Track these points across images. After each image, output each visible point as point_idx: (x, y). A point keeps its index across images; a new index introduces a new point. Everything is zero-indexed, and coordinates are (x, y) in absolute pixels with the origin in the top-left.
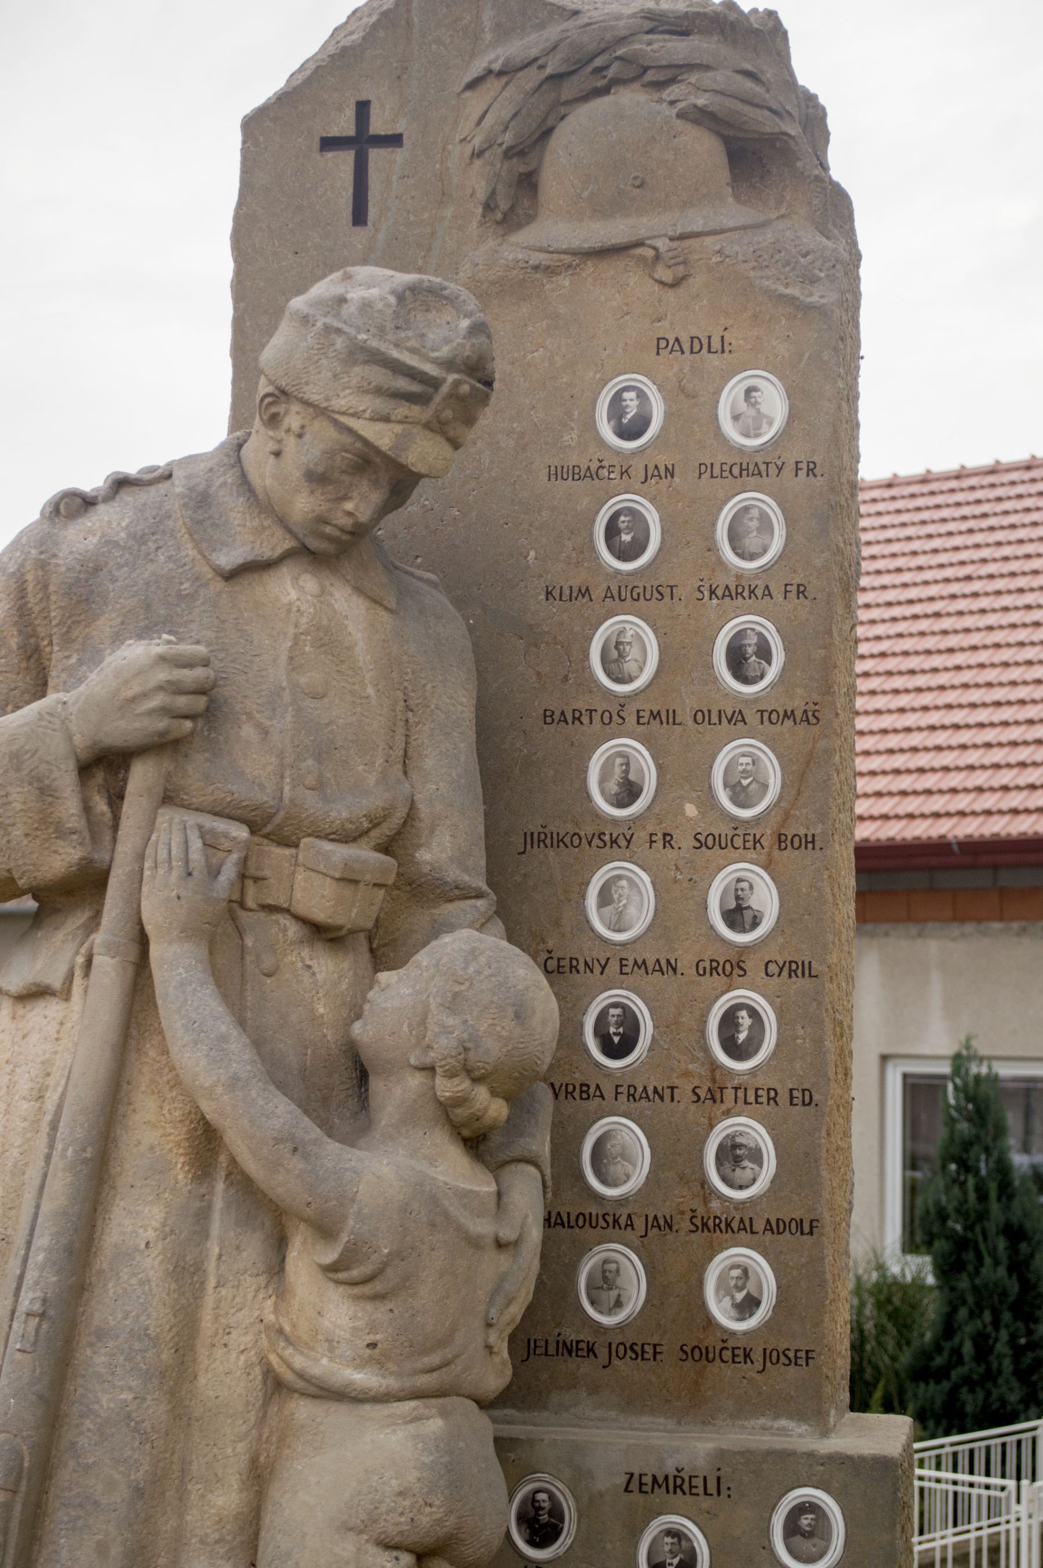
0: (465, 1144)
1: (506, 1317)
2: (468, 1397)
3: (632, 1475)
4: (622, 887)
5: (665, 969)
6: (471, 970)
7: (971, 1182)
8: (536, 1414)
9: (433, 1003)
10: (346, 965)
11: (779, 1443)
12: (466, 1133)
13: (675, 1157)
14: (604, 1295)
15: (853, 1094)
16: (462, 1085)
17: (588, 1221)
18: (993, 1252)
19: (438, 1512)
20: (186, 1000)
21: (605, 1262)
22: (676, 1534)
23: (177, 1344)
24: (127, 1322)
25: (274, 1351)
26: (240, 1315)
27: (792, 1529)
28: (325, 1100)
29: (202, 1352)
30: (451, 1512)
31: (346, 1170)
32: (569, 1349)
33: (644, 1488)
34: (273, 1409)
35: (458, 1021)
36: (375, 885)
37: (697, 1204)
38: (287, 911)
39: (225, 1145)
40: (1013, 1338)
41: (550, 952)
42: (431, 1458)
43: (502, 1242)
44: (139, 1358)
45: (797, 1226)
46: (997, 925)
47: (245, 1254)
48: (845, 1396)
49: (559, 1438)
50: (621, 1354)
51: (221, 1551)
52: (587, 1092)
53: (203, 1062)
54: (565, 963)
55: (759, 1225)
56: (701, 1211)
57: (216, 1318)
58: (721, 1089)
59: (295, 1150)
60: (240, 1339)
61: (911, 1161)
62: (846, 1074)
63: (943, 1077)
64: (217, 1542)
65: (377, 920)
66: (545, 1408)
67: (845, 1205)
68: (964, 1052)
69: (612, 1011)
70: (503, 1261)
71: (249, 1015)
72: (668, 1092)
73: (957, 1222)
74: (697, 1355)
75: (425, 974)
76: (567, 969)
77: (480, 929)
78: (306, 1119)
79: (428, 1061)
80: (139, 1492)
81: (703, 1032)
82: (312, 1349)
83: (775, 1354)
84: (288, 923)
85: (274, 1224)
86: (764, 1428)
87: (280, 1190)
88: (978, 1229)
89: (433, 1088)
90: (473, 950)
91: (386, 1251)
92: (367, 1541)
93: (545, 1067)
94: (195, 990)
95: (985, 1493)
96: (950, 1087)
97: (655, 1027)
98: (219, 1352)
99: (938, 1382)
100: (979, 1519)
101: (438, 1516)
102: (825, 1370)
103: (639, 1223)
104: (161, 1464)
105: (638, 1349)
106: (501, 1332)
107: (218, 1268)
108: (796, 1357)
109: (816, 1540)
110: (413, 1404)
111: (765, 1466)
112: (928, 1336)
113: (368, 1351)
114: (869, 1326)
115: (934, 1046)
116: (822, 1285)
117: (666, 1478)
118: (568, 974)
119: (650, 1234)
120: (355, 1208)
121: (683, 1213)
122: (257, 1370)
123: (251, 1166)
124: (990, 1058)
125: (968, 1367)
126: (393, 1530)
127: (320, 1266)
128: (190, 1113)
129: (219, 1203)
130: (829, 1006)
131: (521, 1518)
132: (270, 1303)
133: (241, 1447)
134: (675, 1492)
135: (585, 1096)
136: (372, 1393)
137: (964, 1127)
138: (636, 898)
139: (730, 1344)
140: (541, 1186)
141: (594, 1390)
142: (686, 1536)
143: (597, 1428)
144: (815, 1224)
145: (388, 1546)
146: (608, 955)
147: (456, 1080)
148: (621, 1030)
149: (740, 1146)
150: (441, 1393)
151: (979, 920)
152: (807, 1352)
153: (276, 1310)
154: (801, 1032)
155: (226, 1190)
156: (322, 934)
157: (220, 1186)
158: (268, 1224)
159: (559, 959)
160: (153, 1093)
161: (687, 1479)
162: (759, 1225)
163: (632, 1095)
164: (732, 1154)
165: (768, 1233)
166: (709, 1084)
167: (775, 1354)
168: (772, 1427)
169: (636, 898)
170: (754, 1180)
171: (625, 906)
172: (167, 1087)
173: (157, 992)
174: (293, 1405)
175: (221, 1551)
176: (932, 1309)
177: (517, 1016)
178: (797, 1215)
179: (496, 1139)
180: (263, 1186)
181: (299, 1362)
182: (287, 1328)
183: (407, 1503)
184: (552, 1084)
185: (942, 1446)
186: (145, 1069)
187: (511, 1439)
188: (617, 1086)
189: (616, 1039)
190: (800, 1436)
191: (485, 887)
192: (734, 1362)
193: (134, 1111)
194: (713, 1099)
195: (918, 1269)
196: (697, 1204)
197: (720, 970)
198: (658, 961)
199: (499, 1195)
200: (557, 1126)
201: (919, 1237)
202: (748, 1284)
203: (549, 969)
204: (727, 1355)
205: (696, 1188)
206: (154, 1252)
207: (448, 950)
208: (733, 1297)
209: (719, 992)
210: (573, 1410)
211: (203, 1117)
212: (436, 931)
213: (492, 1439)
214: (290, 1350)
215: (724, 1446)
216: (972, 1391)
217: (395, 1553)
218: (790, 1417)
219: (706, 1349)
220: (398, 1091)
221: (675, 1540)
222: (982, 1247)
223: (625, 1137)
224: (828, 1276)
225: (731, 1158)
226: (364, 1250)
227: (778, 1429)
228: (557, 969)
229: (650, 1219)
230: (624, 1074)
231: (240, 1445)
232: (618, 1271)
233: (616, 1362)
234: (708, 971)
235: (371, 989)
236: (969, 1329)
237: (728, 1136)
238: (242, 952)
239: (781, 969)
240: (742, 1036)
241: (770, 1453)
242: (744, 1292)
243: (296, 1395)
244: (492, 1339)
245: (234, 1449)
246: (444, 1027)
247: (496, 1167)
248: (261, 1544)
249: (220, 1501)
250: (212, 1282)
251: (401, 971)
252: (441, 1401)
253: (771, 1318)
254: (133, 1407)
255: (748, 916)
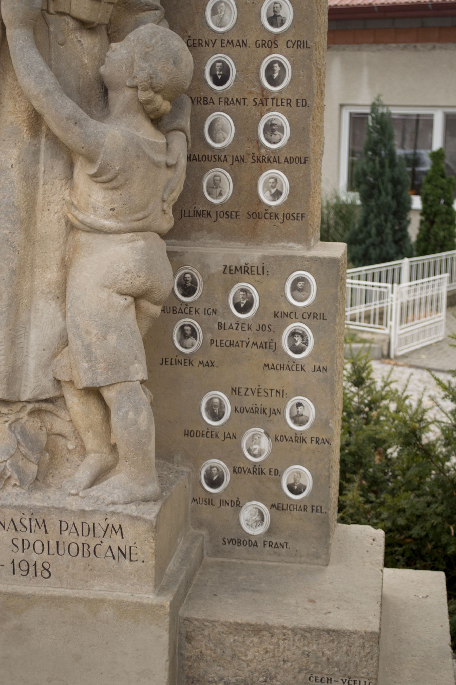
0: (152, 122)
1: (171, 198)
2: (155, 232)
3: (226, 266)
4: (222, 6)
5: (241, 44)
6: (153, 41)
7: (377, 159)
8: (185, 242)
9: (136, 57)
10: (97, 41)
11: (289, 253)
12: (152, 116)
13: (246, 130)
14: (214, 191)
15: (325, 103)
16: (150, 94)
17: (207, 158)
18: (386, 190)
19: (143, 280)
20: (24, 55)
21: (215, 176)
22: (245, 291)
23: (27, 209)
24: (5, 200)
25: (70, 212)
26: (54, 197)
27: (294, 288)
28: (89, 102)
29: (38, 213)
30: (148, 279)
31: (99, 132)
32: (199, 214)
33: (231, 272)
34: (70, 238)
35: (147, 65)
36: (109, 3)
37: (255, 150)
38: (69, 15)
39: (45, 122)
40: (393, 226)
41: (189, 37)
42: (139, 257)
43: (169, 165)
44: (11, 215)
45: (299, 161)
46: (393, 45)
47: (56, 170)
48: (318, 235)
49: (195, 251)
50: (222, 216)
51: (50, 296)
52: (206, 101)
53: (33, 84)
54: (196, 42)
55: (282, 160)
56: (257, 154)
57: (44, 198)
58: (266, 99)
59: (76, 123)
60: (55, 207)
61: (352, 153)
62: (322, 93)
63: (366, 114)
64: (48, 293)
65: (110, 20)
66: (189, 239)
67: (320, 152)
68: (377, 103)
69: (218, 64)
70: (170, 173)
71: (53, 63)
72: (242, 101)
73: (371, 177)
74: (254, 216)
75: (132, 44)
76: (197, 45)
77: (158, 23)
78: (80, 109)
79: (134, 83)
80: (14, 272)
81: (258, 74)
82: (87, 211)
83: (288, 215)
84: (69, 21)
85: (68, 156)
86: (283, 247)
87: (70, 141)
88: (380, 180)
89: (137, 96)
90: (154, 32)
91: (118, 168)
92: (113, 292)
93: (187, 87)
94: (28, 50)
95: (378, 289)
96: (370, 118)
97: (237, 71)
98: (46, 213)
99: (360, 245)
100: (376, 300)
101: (143, 281)
102: (310, 222)
103: (230, 159)
104: (23, 260)
105: (229, 213)
106: (169, 204)
107: (44, 176)
108: (297, 217)
109: (304, 292)
110: (131, 234)
111: (283, 262)
112: (357, 226)
113: (111, 212)
114: (332, 222)
115: (363, 100)
116: (309, 185)
117: (241, 267)
118: (198, 47)
119: (234, 164)
120: (103, 148)
121: (249, 154)
122: (63, 221)
123: (57, 131)
124: (388, 106)
125: (374, 238)
126: (123, 287)
127: (89, 175)
128: (28, 107)
129: (43, 148)
130: (315, 62)
131: (179, 285)
132: (67, 192)
133: (57, 253)
134: (245, 273)
135: (205, 103)
136: (113, 230)
137: (375, 135)
138: (228, 11)
139: (269, 211)
140: (186, 141)
141: (210, 231)
142: (249, 291)
143: (212, 247)
144: (306, 159)
145: (122, 294)
146: (216, 38)
147: (147, 92)
148: (222, 73)
149: (274, 125)
150: (143, 230)
151: (385, 43)
152: (302, 214)
153: (70, 195)
154: (302, 73)
155: (46, 142)
156: (86, 26)
157: (43, 140)
158: (65, 157)
159: (194, 40)
160: (11, 98)
161: (250, 268)
162: (282, 160)
163: (226, 102)
164: (270, 128)
165: (286, 163)
166: (261, 97)
167: (288, 215)
168: (286, 246)
169: (228, 11)
170: (280, 140)
171: (223, 15)
172: (17, 96)
173: (11, 52)
174: (79, 235)
175: (50, 296)
176: (359, 215)
177: (174, 63)
178: (299, 155)
179: (166, 120)
180: (62, 140)
181: (81, 216)
182: (75, 203)
183: (129, 276)
184: (191, 98)
185: (361, 271)
186: (7, 87)
187: (174, 252)
188: (220, 98)
189: (219, 77)
190: (299, 250)
191: (159, 5)
192: (270, 219)
193: (3, 106)
194: (263, 104)
195: (353, 198)
196: (255, 150)
197: (266, 45)
198: (238, 41)
199: (167, 145)
200: (193, 116)
201: (354, 184)
202: (277, 185)
203: (189, 45)
204: (268, 216)
205: (255, 144)
206: (15, 169)
207: (143, 32)
208: (270, 191)
209: (265, 55)
210: (201, 240)
211: (34, 109)
212: (137, 25)
213: (166, 252)
214: (77, 212)
215: (266, 254)
216: (375, 249)
217: (125, 297)
218: (294, 242)
219: (259, 213)
220: (121, 97)
221: (245, 293)
222: (382, 188)
223: (224, 121)
224: (312, 182)
225: (270, 130)
226: (108, 167)
227: (289, 247)
228: (193, 44)
229: (235, 157)
230: (223, 93)
231: (56, 252)
232: (220, 180)
233: (220, 219)
234: (261, 45)
235: (108, 50)
236: (374, 222)
237: (269, 120)
238: (49, 33)
239: (294, 44)
240: (276, 75)
241: (285, 256)
242: (275, 189)
243: (80, 231)
244: (165, 207)
245: (54, 254)
246: (141, 68)
247: (166, 132)
248: (67, 293)
249: (49, 276)
250: (41, 182)
251: (122, 43)
252: (143, 233)
253: (287, 200)
254: (9, 236)
255: (279, 19)
